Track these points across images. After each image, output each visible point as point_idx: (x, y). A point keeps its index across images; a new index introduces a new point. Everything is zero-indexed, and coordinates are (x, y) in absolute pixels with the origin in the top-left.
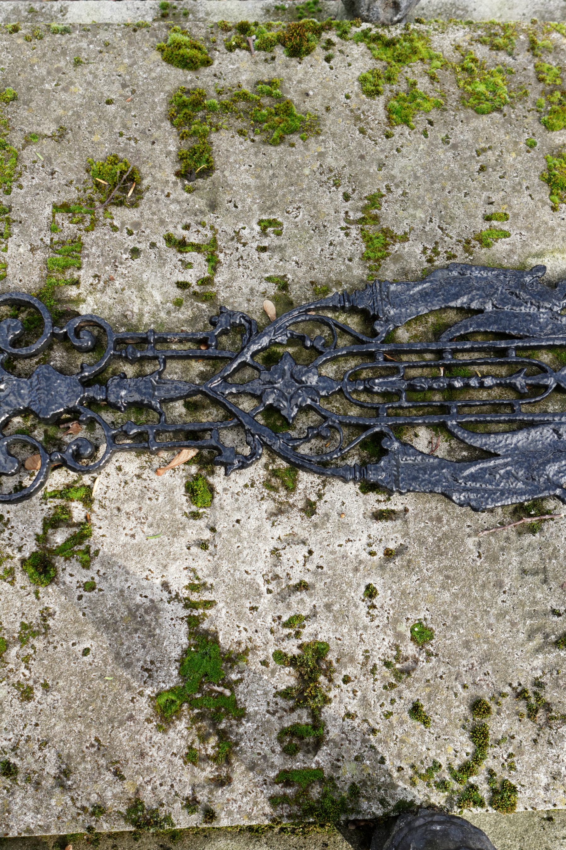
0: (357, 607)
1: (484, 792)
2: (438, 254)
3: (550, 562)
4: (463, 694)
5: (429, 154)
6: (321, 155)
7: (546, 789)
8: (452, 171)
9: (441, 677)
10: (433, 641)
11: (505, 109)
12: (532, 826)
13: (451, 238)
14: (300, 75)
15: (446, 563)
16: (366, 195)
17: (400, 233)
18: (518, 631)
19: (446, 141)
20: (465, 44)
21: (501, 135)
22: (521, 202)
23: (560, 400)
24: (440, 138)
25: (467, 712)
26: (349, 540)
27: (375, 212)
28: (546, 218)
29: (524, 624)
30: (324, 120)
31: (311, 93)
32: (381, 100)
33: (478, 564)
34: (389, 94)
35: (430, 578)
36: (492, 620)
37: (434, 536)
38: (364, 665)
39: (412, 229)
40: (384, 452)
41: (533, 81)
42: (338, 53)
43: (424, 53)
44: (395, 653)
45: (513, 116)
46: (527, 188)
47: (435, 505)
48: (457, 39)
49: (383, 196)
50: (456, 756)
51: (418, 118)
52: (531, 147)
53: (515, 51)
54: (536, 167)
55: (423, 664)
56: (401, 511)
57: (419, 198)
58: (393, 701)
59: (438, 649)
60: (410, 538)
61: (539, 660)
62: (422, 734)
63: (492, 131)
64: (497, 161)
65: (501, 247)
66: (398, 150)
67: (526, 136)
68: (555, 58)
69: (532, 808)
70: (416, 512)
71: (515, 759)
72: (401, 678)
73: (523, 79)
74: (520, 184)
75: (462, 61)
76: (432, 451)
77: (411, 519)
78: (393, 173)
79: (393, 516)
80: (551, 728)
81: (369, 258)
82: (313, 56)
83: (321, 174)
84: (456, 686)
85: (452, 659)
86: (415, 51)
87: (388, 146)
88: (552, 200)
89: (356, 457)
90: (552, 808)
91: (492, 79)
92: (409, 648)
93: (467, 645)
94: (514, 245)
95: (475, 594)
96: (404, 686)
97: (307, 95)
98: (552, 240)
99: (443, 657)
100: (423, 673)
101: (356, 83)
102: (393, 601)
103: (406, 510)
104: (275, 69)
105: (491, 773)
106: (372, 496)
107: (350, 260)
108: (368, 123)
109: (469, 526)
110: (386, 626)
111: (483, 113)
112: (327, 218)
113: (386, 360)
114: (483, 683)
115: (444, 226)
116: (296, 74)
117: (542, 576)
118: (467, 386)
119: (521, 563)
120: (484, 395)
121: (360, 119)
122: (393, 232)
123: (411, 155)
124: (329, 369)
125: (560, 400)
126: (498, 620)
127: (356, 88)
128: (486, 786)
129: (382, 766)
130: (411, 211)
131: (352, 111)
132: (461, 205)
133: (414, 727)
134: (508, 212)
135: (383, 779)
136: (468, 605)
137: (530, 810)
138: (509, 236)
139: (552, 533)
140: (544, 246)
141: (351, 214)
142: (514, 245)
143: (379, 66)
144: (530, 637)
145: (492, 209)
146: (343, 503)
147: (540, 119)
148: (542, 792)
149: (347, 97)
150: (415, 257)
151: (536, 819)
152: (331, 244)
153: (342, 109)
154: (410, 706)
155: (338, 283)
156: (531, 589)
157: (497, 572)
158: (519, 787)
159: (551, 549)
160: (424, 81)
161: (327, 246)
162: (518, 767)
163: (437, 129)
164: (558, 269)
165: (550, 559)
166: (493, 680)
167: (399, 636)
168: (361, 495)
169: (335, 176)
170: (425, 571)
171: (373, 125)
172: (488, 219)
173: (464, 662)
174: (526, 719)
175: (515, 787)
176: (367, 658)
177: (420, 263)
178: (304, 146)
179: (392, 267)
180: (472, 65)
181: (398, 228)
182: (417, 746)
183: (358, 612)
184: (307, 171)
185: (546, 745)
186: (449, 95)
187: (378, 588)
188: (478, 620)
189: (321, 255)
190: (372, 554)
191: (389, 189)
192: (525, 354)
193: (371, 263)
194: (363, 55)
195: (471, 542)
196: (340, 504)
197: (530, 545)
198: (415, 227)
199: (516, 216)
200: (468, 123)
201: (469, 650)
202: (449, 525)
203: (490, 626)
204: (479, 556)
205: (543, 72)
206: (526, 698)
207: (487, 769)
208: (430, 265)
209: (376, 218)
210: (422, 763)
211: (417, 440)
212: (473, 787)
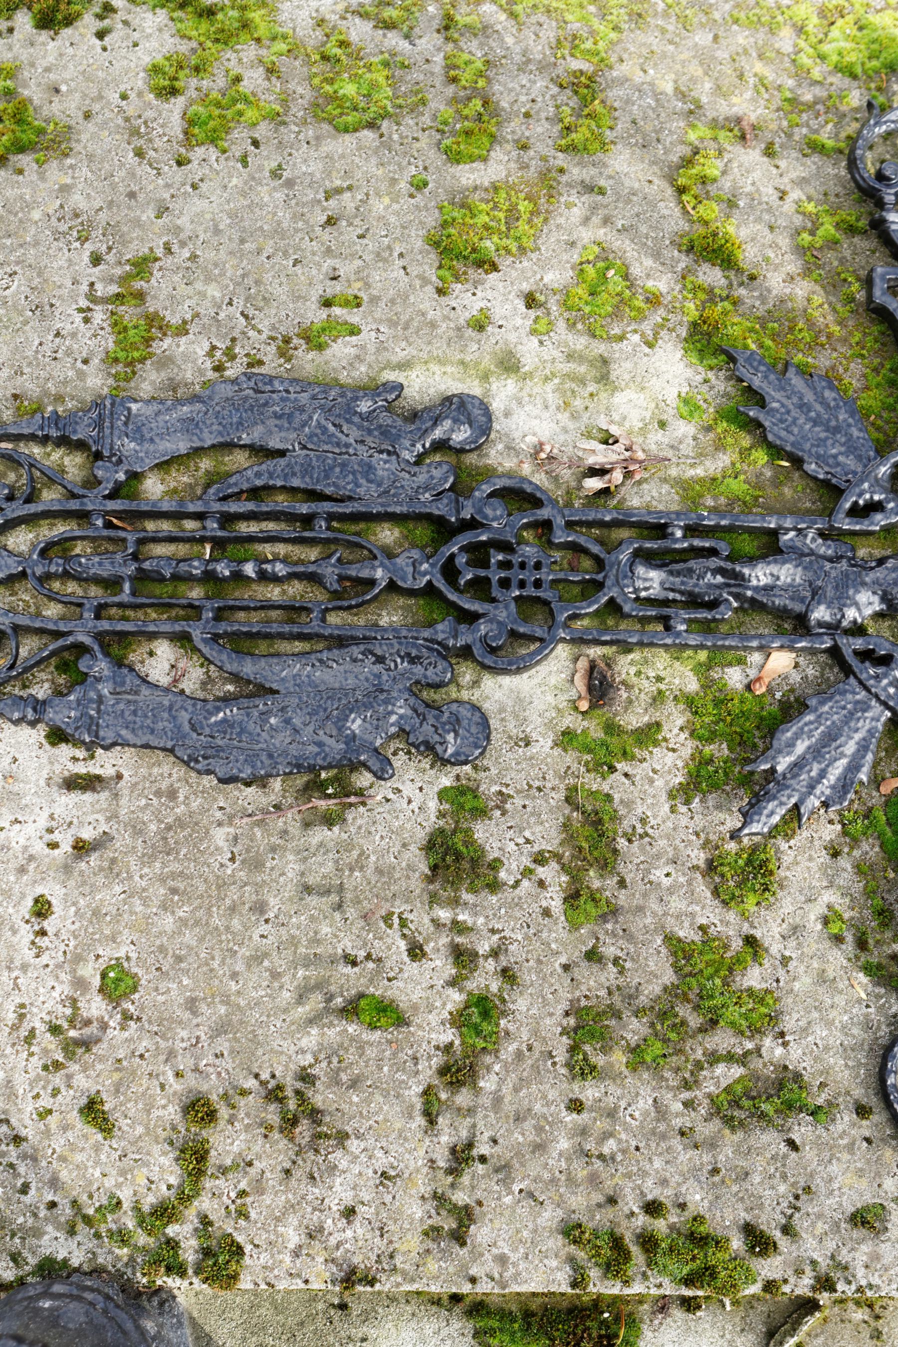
0: (15, 932)
1: (189, 1253)
2: (233, 358)
3: (350, 876)
4: (175, 1086)
5: (244, 195)
6: (65, 189)
7: (296, 1253)
8: (279, 223)
9: (141, 1056)
10: (136, 996)
11: (385, 124)
12: (312, 1317)
13: (259, 332)
14: (51, 59)
15: (175, 867)
16: (128, 257)
17: (175, 320)
18: (281, 987)
19: (276, 174)
20: (334, 17)
21: (372, 167)
22: (387, 279)
23: (401, 608)
24: (267, 169)
25: (178, 1118)
26: (17, 821)
27: (138, 284)
28: (425, 306)
29: (294, 976)
30: (79, 133)
31: (64, 88)
32: (179, 102)
33: (229, 872)
34: (195, 94)
35: (144, 890)
36: (240, 967)
37: (160, 821)
38: (15, 1028)
39: (197, 315)
40: (82, 679)
41: (438, 81)
42: (120, 26)
43: (262, 31)
44: (68, 1011)
45: (395, 137)
46: (401, 255)
47: (168, 771)
48: (322, 9)
49: (156, 259)
50: (149, 1189)
51: (235, 134)
52: (418, 188)
53: (417, 30)
54: (421, 222)
55: (114, 1032)
56: (111, 778)
57: (216, 265)
58: (56, 1092)
59: (142, 1009)
60: (118, 823)
61: (311, 1039)
62: (97, 1148)
63: (357, 160)
64: (357, 209)
65: (341, 351)
66: (194, 187)
67: (413, 170)
68: (481, 45)
69: (268, 1284)
70: (134, 780)
71: (249, 1200)
72: (74, 1053)
73: (422, 77)
74: (389, 248)
75: (324, 44)
76: (176, 681)
77: (126, 792)
78: (179, 222)
79: (97, 785)
80: (317, 1151)
81: (116, 360)
82: (76, 28)
83: (59, 220)
84: (164, 1073)
85: (164, 1027)
86: (245, 25)
87: (178, 178)
88: (440, 278)
89: (46, 685)
90: (302, 1286)
91: (368, 75)
92: (94, 1005)
93: (192, 1005)
94: (363, 347)
95: (216, 921)
96: (77, 1067)
97: (57, 91)
98: (429, 343)
99: (150, 1022)
100: (112, 1047)
101: (142, 74)
102: (77, 924)
103: (119, 777)
104: (10, 48)
105: (205, 1221)
106: (65, 751)
107: (85, 362)
108: (150, 140)
109: (221, 808)
110: (59, 966)
111: (346, 131)
112: (57, 292)
113: (109, 525)
114: (211, 1070)
115: (251, 312)
116: (44, 57)
117: (334, 898)
118: (238, 577)
119: (302, 874)
120: (274, 593)
121: (138, 133)
122: (163, 319)
123: (215, 194)
124: (21, 539)
125: (401, 608)
126: (249, 966)
127: (140, 83)
128: (194, 1243)
129: (23, 1198)
130: (199, 286)
131: (127, 120)
132: (284, 280)
133: (85, 1137)
134: (361, 294)
135: (21, 1220)
136: (201, 940)
137: (263, 1286)
138: (359, 332)
139: (360, 828)
140: (415, 353)
141: (99, 286)
142: (363, 347)
143: (184, 47)
144: (301, 999)
145: (337, 288)
146: (15, 760)
147: (439, 142)
148: (288, 1259)
149: (124, 97)
150: (194, 361)
151: (321, 1306)
152: (58, 334)
153: (112, 115)
154: (84, 1101)
155: (59, 398)
156: (312, 919)
157: (258, 887)
158: (248, 1248)
159: (355, 853)
160: (255, 75)
161: (51, 338)
162: (253, 1215)
163: (265, 153)
164: (432, 391)
165: (352, 870)
166: (229, 1066)
167: (80, 984)
168: (47, 746)
169: (82, 224)
170: (137, 878)
171: (158, 143)
172: (327, 303)
173: (184, 1034)
174: (276, 1135)
175: (240, 1248)
176: (22, 1017)
177: (201, 372)
178: (38, 173)
179: (153, 376)
180: (338, 51)
181: (173, 312)
182: (86, 1168)
183: (15, 940)
184: (36, 215)
185: (305, 1180)
186: (294, 99)
187: (54, 902)
188: (215, 964)
189: (37, 352)
190: (53, 846)
191: (168, 249)
192: (354, 528)
193: (120, 367)
194: (160, 30)
195: (220, 836)
196: (9, 759)
197: (321, 844)
198: (203, 312)
199: (374, 300)
200: (318, 146)
201: (195, 1013)
202: (187, 805)
203: (234, 976)
204: (232, 859)
205: (458, 67)
206: (281, 1100)
207: (199, 1214)
208: (217, 375)
209: (140, 296)
210: (91, 1197)
211: (153, 661)
212: (172, 1244)
